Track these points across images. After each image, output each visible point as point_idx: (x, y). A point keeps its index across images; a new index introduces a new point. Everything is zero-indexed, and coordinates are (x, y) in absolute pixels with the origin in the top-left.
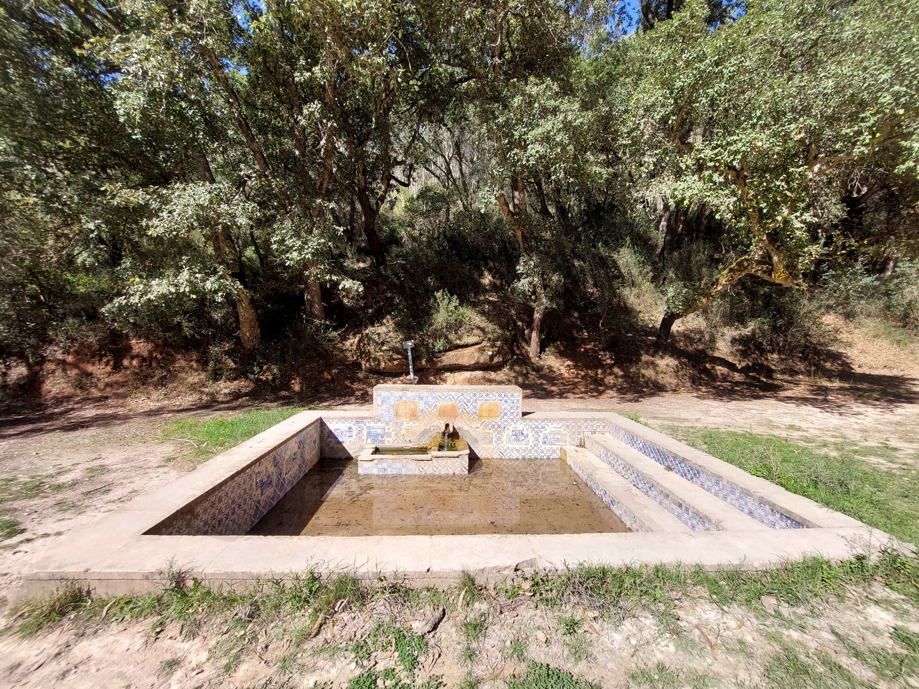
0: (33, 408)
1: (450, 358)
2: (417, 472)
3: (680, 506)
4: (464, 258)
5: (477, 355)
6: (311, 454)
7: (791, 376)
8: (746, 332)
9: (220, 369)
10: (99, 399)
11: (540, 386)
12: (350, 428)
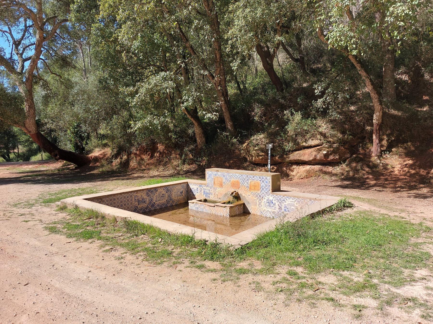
2: (209, 212)
12: (197, 188)
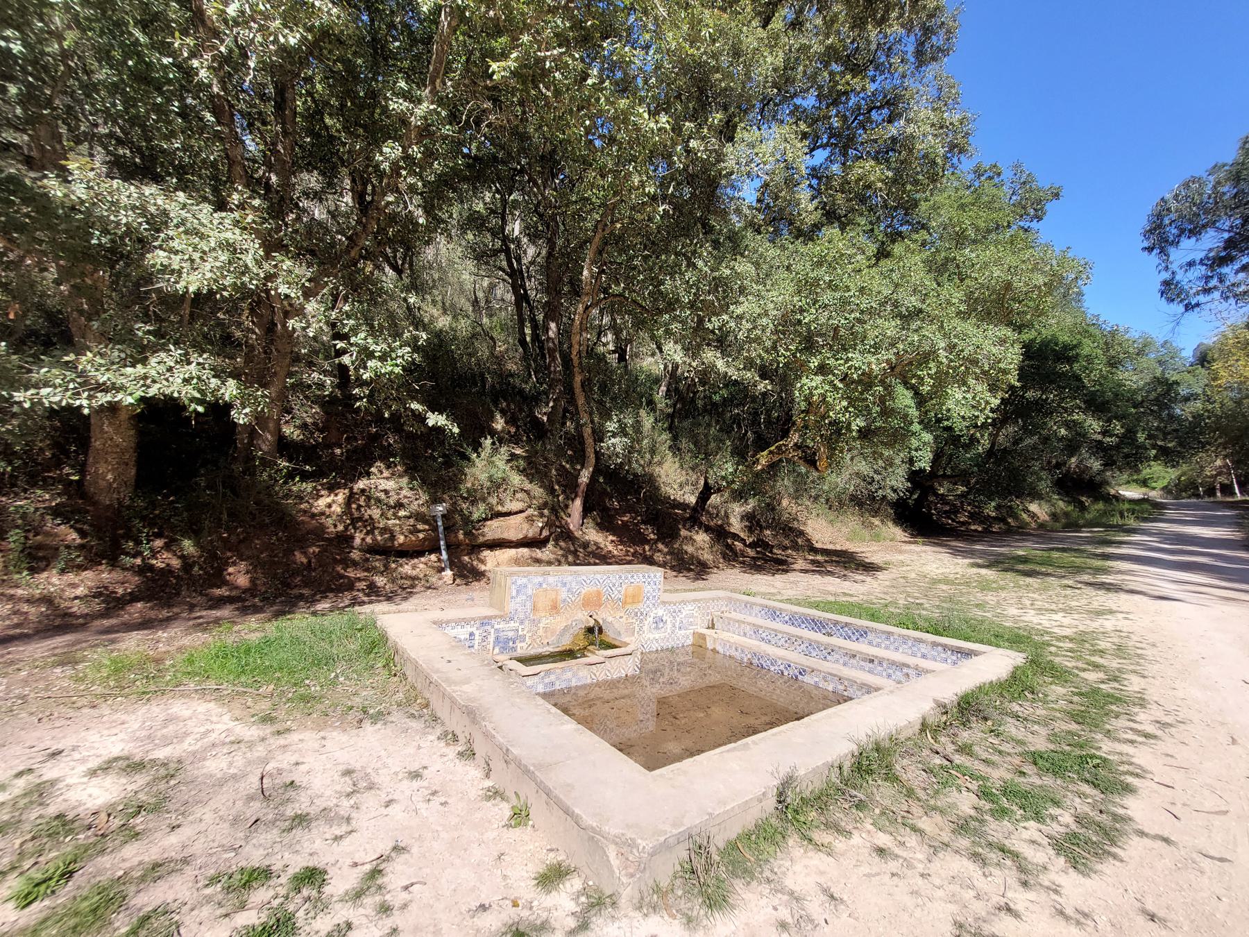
1: (493, 529)
2: (589, 681)
3: (872, 661)
5: (526, 526)
8: (749, 508)
12: (472, 634)
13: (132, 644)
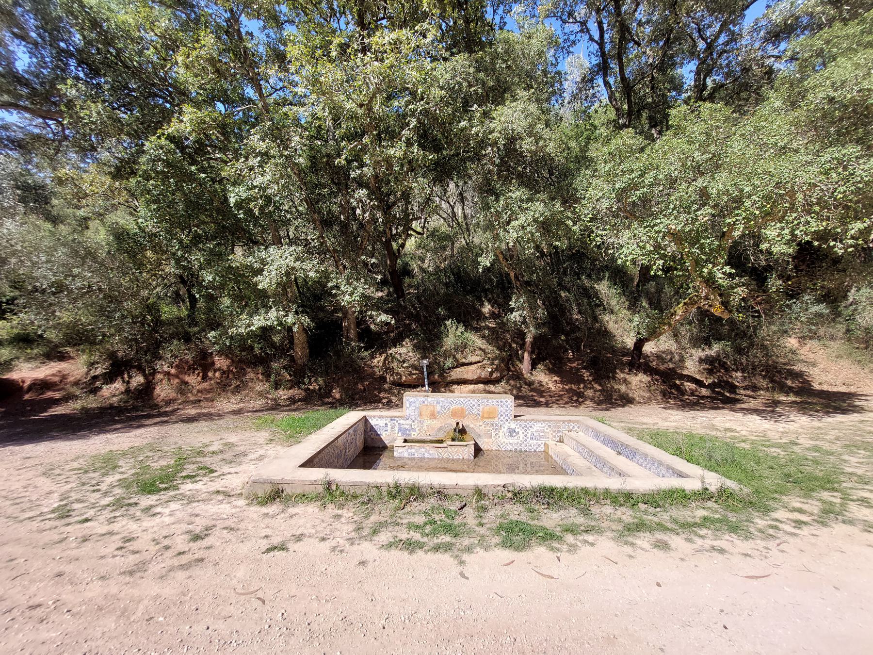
0: (151, 407)
1: (457, 373)
2: (437, 456)
4: (466, 292)
5: (479, 371)
6: (360, 442)
7: (753, 391)
9: (280, 380)
10: (195, 402)
11: (530, 397)
13: (296, 415)
